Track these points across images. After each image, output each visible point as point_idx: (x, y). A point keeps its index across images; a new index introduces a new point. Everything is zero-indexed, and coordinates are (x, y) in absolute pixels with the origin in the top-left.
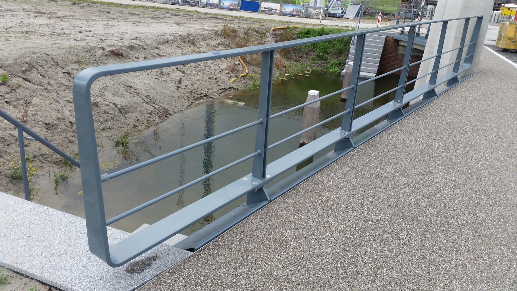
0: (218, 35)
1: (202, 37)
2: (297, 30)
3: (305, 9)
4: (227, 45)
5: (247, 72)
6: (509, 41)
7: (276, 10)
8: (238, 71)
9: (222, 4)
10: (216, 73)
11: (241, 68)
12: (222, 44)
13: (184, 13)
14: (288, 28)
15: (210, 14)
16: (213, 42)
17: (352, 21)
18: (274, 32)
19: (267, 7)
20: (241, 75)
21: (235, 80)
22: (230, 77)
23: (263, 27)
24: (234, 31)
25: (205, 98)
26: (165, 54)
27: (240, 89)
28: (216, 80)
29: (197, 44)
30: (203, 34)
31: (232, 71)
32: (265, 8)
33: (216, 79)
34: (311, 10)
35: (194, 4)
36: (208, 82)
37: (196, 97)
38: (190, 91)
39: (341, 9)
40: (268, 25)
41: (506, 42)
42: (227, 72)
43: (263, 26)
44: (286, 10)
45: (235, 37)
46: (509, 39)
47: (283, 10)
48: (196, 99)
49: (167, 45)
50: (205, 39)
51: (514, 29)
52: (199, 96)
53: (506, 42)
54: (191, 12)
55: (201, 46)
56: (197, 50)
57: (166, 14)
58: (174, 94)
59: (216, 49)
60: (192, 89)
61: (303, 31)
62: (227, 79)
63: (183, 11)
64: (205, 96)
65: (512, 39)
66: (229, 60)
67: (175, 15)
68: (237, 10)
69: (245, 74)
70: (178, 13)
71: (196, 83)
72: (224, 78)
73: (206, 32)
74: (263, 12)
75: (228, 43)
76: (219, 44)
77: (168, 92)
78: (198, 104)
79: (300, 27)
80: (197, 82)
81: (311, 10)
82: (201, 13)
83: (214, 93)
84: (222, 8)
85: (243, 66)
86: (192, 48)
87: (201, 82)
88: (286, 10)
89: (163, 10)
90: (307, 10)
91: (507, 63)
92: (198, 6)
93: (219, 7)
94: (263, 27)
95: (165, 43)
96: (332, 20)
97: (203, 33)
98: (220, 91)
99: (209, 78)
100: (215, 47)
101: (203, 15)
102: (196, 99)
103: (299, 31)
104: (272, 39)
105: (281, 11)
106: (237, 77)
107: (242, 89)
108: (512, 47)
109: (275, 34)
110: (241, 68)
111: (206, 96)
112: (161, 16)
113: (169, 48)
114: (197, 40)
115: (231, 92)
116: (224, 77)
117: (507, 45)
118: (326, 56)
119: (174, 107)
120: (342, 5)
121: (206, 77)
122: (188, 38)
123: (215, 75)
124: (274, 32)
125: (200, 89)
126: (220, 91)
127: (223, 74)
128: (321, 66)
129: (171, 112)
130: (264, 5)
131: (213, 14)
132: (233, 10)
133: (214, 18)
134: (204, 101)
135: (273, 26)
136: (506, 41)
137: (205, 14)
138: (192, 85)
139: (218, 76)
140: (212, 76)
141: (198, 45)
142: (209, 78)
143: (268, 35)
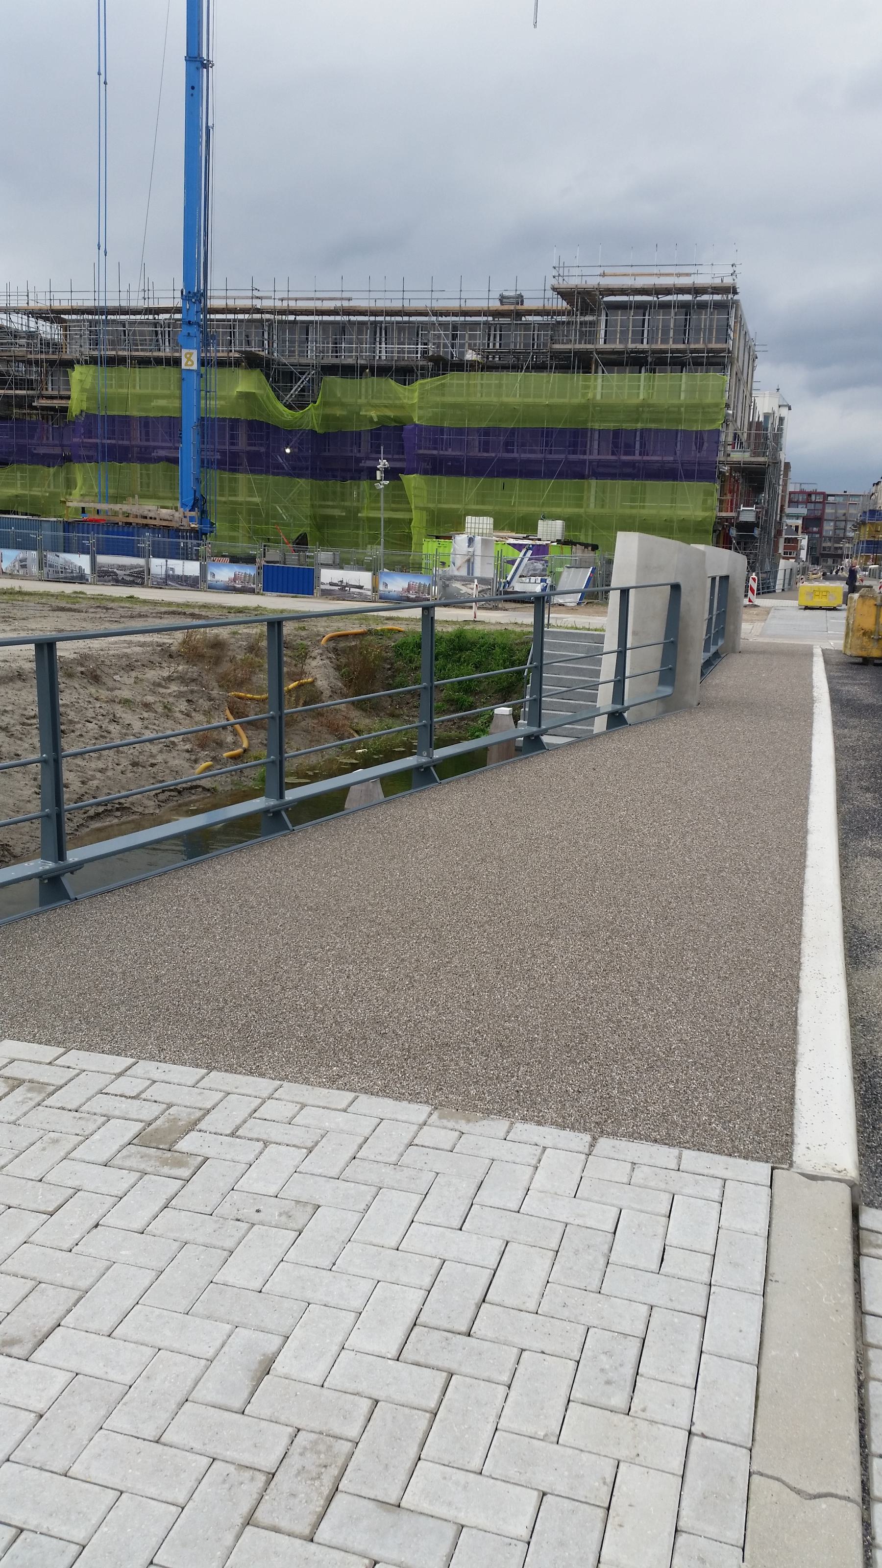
0: (171, 656)
1: (124, 662)
2: (396, 636)
3: (440, 583)
4: (193, 680)
5: (245, 745)
6: (865, 639)
7: (361, 587)
8: (220, 744)
9: (209, 578)
10: (154, 751)
11: (230, 739)
12: (178, 678)
13: (92, 602)
14: (369, 632)
15: (170, 604)
16: (152, 675)
17: (572, 610)
18: (332, 644)
19: (336, 581)
20: (225, 755)
21: (208, 768)
22: (196, 761)
23: (303, 633)
24: (218, 645)
25: (118, 814)
26: (9, 708)
27: (220, 789)
28: (154, 769)
29: (105, 679)
30: (126, 656)
31: (203, 746)
32: (331, 584)
33: (153, 765)
34: (457, 585)
35: (128, 578)
36: (130, 775)
37: (92, 812)
38: (75, 796)
39: (542, 581)
40: (320, 626)
41: (859, 642)
42: (188, 747)
43: (304, 629)
44: (390, 588)
45: (217, 661)
46: (864, 634)
47: (381, 588)
48: (91, 818)
49: (19, 684)
50: (130, 667)
51: (873, 610)
52: (101, 809)
53: (859, 642)
54: (113, 600)
55: (118, 686)
56: (104, 694)
57: (39, 607)
58: (29, 805)
59: (162, 690)
60: (83, 791)
61: (410, 639)
62: (187, 765)
63: (93, 598)
64: (118, 809)
65: (872, 633)
66: (197, 719)
67: (63, 609)
68: (252, 591)
69: (240, 750)
70: (74, 603)
71: (93, 778)
72: (177, 762)
73: (138, 649)
74: (326, 594)
75: (195, 675)
76: (170, 679)
77: (11, 801)
78: (99, 830)
79: (402, 628)
80: (98, 775)
81: (457, 585)
82: (145, 602)
83: (146, 802)
84: (212, 588)
85: (235, 733)
86: (93, 690)
87: (110, 773)
88: (390, 588)
89: (32, 598)
90: (445, 587)
91: (632, 663)
92: (142, 585)
93: (201, 585)
94: (303, 633)
95: (11, 679)
96: (514, 609)
97: (128, 651)
98: (162, 797)
99: (135, 764)
100: (159, 685)
101: (145, 609)
102: (91, 818)
103: (400, 638)
104: (327, 661)
105: (375, 589)
106: (214, 759)
107: (229, 788)
108: (875, 653)
109: (335, 650)
110: (230, 739)
111: (122, 809)
112: (19, 614)
113: (23, 693)
114: (106, 669)
115: (193, 797)
116: (177, 761)
117: (862, 648)
118: (471, 699)
119: (26, 838)
120: (544, 570)
121: (125, 762)
122: (82, 665)
123: (152, 756)
124: (332, 644)
125: (106, 791)
126: (162, 797)
127: (175, 753)
128: (459, 728)
129: (17, 851)
130: (328, 576)
131: (178, 605)
132: (243, 591)
133: (173, 613)
134: (116, 821)
135: (329, 628)
136: (858, 638)
137: (155, 603)
138: (83, 783)
139: (160, 758)
140: (142, 758)
141: (110, 684)
142: (135, 764)
143: (316, 652)
